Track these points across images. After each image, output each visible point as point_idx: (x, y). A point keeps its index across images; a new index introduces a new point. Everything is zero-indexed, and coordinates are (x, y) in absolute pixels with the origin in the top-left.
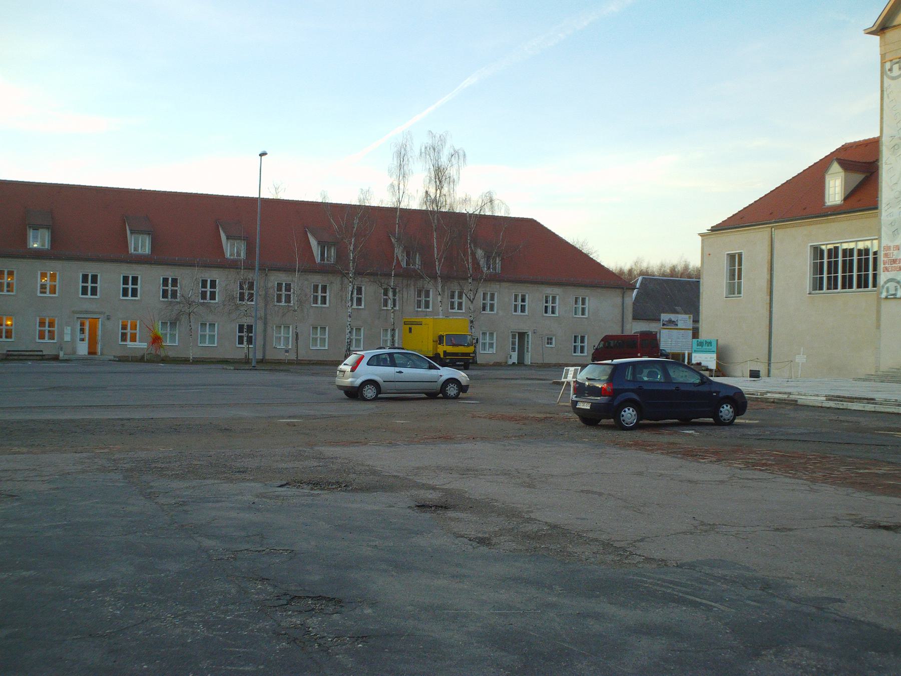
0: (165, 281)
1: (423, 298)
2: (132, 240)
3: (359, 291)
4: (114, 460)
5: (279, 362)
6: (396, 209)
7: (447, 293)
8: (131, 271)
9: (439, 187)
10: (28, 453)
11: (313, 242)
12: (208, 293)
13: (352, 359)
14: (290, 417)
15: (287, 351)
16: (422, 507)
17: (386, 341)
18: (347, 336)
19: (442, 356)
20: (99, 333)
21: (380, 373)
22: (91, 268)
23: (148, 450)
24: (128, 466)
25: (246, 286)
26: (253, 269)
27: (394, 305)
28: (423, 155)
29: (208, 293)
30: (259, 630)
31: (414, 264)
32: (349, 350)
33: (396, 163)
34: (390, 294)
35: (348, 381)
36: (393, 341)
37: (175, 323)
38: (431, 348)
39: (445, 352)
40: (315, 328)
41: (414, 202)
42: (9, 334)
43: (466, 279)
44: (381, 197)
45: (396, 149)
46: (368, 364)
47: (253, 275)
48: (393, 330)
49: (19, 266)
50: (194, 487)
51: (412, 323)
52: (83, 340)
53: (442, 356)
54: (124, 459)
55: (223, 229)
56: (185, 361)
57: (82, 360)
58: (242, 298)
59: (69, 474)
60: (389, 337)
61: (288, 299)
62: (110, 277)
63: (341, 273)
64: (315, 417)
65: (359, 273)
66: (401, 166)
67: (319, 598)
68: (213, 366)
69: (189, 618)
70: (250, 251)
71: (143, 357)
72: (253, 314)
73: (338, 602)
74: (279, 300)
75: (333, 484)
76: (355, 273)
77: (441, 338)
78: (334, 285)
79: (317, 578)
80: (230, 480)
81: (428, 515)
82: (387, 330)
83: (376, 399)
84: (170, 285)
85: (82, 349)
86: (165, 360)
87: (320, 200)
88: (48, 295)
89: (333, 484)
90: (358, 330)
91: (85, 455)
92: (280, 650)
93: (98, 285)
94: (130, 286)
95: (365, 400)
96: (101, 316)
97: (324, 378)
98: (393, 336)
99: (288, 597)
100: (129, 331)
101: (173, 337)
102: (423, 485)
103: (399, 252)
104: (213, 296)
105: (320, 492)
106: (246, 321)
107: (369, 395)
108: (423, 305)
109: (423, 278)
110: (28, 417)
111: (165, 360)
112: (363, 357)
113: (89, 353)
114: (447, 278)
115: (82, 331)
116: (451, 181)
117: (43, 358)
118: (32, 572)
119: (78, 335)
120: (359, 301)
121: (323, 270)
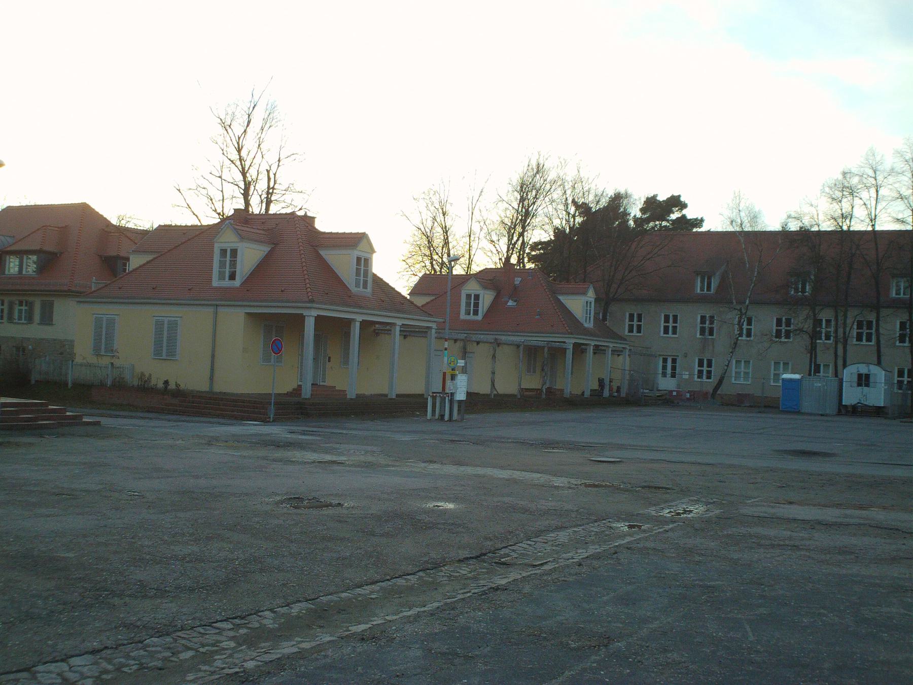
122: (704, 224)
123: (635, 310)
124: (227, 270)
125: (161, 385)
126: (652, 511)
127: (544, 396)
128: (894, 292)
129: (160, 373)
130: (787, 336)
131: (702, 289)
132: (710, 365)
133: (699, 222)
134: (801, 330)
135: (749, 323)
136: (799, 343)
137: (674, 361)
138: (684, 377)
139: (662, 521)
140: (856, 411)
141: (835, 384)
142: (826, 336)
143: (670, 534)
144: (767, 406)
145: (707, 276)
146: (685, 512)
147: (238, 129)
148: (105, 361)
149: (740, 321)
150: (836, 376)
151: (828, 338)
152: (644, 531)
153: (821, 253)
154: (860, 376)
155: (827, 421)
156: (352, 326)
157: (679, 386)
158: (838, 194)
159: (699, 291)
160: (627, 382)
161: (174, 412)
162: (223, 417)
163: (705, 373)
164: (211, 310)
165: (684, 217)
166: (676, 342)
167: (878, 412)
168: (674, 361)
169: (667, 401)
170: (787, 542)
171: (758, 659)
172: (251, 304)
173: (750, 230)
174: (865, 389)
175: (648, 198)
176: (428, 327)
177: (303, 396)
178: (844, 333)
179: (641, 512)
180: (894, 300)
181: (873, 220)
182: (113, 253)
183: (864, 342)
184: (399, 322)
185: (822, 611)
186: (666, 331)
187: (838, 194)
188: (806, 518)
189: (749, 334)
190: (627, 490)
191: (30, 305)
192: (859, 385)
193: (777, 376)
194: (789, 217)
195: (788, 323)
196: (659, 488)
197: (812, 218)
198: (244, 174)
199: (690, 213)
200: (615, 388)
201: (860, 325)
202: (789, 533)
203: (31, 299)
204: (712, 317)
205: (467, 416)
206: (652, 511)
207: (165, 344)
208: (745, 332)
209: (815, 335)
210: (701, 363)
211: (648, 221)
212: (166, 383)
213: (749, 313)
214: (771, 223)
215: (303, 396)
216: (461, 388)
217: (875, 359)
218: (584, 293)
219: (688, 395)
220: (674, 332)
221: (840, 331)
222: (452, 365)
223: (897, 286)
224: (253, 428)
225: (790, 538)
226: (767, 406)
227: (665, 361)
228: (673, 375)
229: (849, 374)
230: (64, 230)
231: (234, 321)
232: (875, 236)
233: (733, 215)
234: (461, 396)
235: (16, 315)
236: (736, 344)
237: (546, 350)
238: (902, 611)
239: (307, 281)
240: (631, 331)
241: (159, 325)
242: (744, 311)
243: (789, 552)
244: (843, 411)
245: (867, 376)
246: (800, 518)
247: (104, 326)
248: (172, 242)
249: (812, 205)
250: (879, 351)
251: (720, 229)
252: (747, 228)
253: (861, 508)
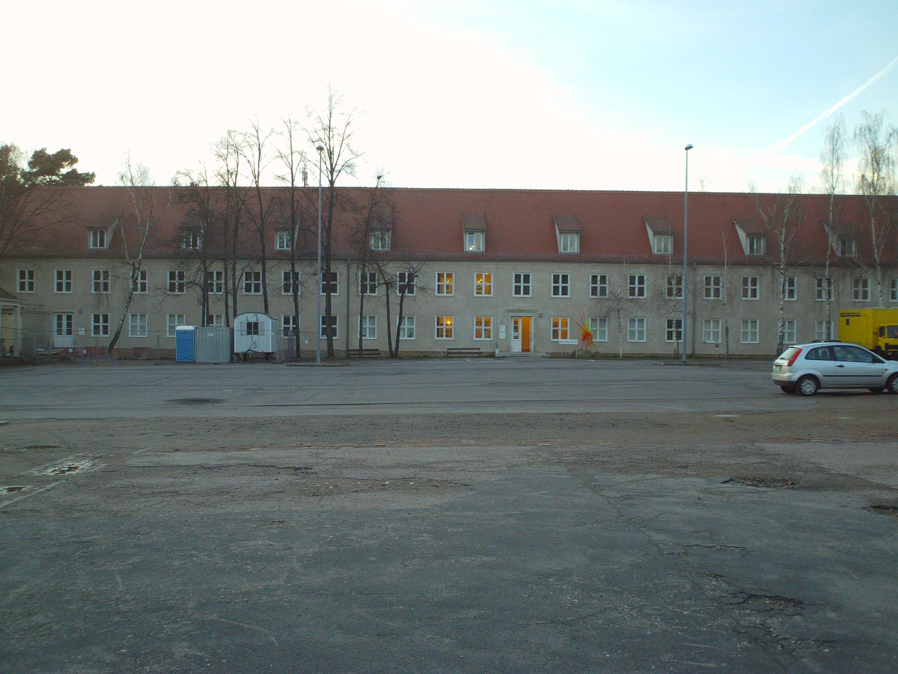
0: (594, 278)
1: (860, 289)
2: (561, 240)
3: (791, 282)
4: (557, 453)
5: (709, 357)
6: (829, 195)
7: (888, 282)
8: (560, 269)
9: (877, 168)
10: (476, 445)
11: (742, 234)
12: (637, 290)
13: (788, 353)
14: (726, 413)
15: (717, 346)
16: (879, 508)
17: (821, 334)
18: (780, 330)
19: (883, 349)
20: (532, 330)
21: (819, 367)
22: (523, 269)
23: (588, 444)
24: (570, 459)
25: (674, 282)
26: (681, 263)
27: (830, 297)
28: (858, 137)
29: (637, 290)
30: (718, 627)
31: (850, 252)
32: (781, 344)
33: (828, 147)
34: (825, 284)
35: (785, 375)
36: (829, 334)
37: (605, 320)
38: (871, 341)
39: (886, 344)
40: (745, 322)
41: (849, 187)
42: (449, 333)
43: (823, 265)
44: (813, 184)
45: (828, 133)
46: (807, 358)
47: (683, 271)
48: (829, 322)
49: (458, 269)
50: (637, 481)
51: (849, 315)
52: (516, 338)
53: (883, 349)
54: (566, 452)
55: (739, 224)
56: (616, 357)
57: (515, 356)
58: (670, 293)
59: (515, 465)
60: (824, 330)
61: (717, 292)
62: (541, 277)
63: (772, 265)
64: (752, 413)
65: (791, 264)
66: (834, 151)
67: (778, 598)
68: (643, 362)
69: (646, 611)
70: (678, 246)
71: (574, 353)
72: (683, 309)
73: (799, 603)
74: (708, 295)
75: (778, 481)
76: (786, 265)
77: (881, 331)
78: (765, 278)
79: (772, 577)
80: (673, 475)
81: (885, 517)
82: (821, 323)
83: (815, 394)
84: (599, 282)
85: (517, 346)
86: (595, 356)
87: (747, 191)
88: (483, 295)
89: (778, 481)
90: (791, 323)
91: (529, 448)
92: (741, 648)
93: (530, 285)
94: (560, 285)
95: (803, 395)
96: (534, 314)
97: (754, 374)
98: (829, 328)
99: (744, 596)
100: (560, 328)
101: (603, 333)
102: (877, 484)
103: (834, 242)
104: (641, 292)
105: (766, 489)
106: (674, 316)
107: (808, 390)
108: (861, 295)
109: (860, 266)
110: (474, 411)
111: (595, 356)
112: (800, 351)
113: (523, 350)
114: (887, 266)
115: (516, 329)
116: (890, 162)
117: (480, 355)
118: (492, 558)
119: (513, 334)
120: (791, 293)
121: (752, 262)
123: (27, 267)
126: (35, 472)
130: (181, 290)
133: (90, 177)
134: (193, 283)
135: (143, 278)
136: (192, 296)
137: (69, 318)
139: (46, 480)
140: (246, 358)
141: (227, 334)
142: (481, 289)
143: (52, 493)
144: (164, 357)
145: (99, 232)
146: (70, 469)
149: (133, 276)
150: (228, 325)
151: (219, 289)
152: (25, 493)
153: (210, 208)
154: (249, 325)
155: (221, 369)
157: (75, 343)
158: (224, 152)
159: (91, 247)
160: (20, 342)
163: (101, 328)
165: (74, 171)
167: (267, 357)
168: (69, 318)
169: (63, 358)
170: (168, 489)
171: (125, 609)
173: (140, 185)
174: (255, 336)
175: (36, 152)
178: (234, 284)
179: (22, 473)
180: (278, 252)
181: (256, 177)
183: (253, 293)
185: (193, 552)
186: (60, 287)
187: (224, 152)
188: (190, 463)
189: (143, 288)
190: (11, 453)
192: (249, 333)
193: (172, 328)
194: (178, 173)
195: (181, 276)
196: (45, 447)
197: (200, 174)
199: (81, 168)
200: (8, 349)
201: (248, 277)
202: (171, 480)
204: (106, 273)
206: (35, 472)
208: (139, 286)
209: (206, 288)
210: (97, 319)
211: (36, 175)
213: (144, 267)
214: (161, 179)
219: (85, 352)
220: (68, 289)
221: (230, 282)
223: (281, 238)
225: (172, 485)
226: (164, 357)
227: (60, 318)
228: (69, 332)
229: (239, 324)
232: (258, 192)
233: (124, 170)
236: (130, 298)
238: (267, 542)
240: (22, 288)
242: (137, 266)
243: (169, 498)
244: (236, 359)
245: (256, 325)
246: (184, 464)
252: (138, 184)
253: (242, 449)
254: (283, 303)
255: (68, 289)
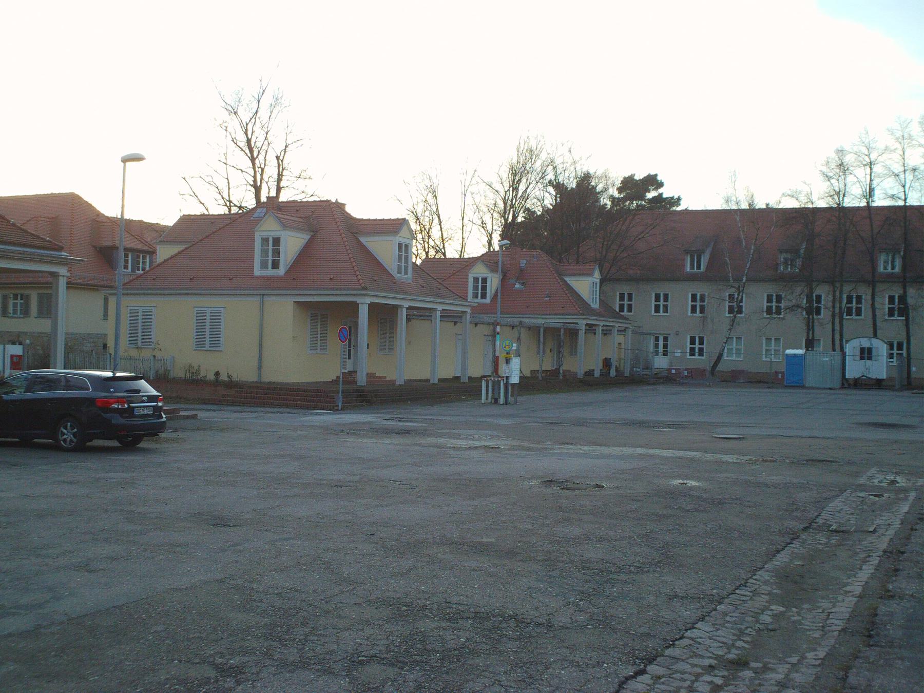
122: (682, 202)
123: (626, 289)
124: (270, 259)
125: (211, 377)
127: (561, 377)
128: (882, 267)
129: (209, 365)
131: (692, 268)
132: (701, 343)
134: (798, 306)
136: (796, 322)
137: (666, 339)
138: (677, 355)
140: (858, 384)
147: (245, 116)
148: (146, 354)
154: (862, 350)
156: (399, 311)
159: (688, 270)
161: (233, 404)
162: (287, 406)
163: (697, 350)
164: (257, 299)
166: (672, 320)
167: (878, 384)
168: (666, 339)
169: (668, 379)
172: (301, 292)
174: (869, 362)
175: (625, 178)
176: (463, 312)
177: (359, 384)
182: (106, 243)
184: (440, 308)
186: (657, 309)
191: (26, 299)
192: (862, 358)
198: (253, 160)
199: (667, 192)
203: (26, 292)
205: (520, 399)
207: (208, 334)
210: (693, 341)
212: (217, 374)
215: (359, 384)
216: (514, 371)
217: (871, 333)
218: (591, 274)
222: (507, 349)
224: (322, 418)
227: (657, 339)
228: (665, 354)
229: (852, 348)
230: (54, 222)
231: (283, 312)
234: (515, 380)
235: (11, 310)
237: (562, 331)
239: (356, 268)
241: (201, 316)
244: (846, 385)
245: (870, 350)
247: (140, 317)
248: (195, 231)
249: (805, 183)
250: (875, 325)
251: (720, 208)
254: (894, 328)
255: (666, 311)
